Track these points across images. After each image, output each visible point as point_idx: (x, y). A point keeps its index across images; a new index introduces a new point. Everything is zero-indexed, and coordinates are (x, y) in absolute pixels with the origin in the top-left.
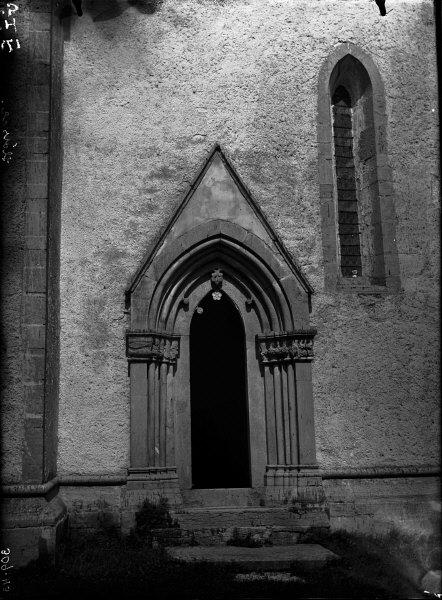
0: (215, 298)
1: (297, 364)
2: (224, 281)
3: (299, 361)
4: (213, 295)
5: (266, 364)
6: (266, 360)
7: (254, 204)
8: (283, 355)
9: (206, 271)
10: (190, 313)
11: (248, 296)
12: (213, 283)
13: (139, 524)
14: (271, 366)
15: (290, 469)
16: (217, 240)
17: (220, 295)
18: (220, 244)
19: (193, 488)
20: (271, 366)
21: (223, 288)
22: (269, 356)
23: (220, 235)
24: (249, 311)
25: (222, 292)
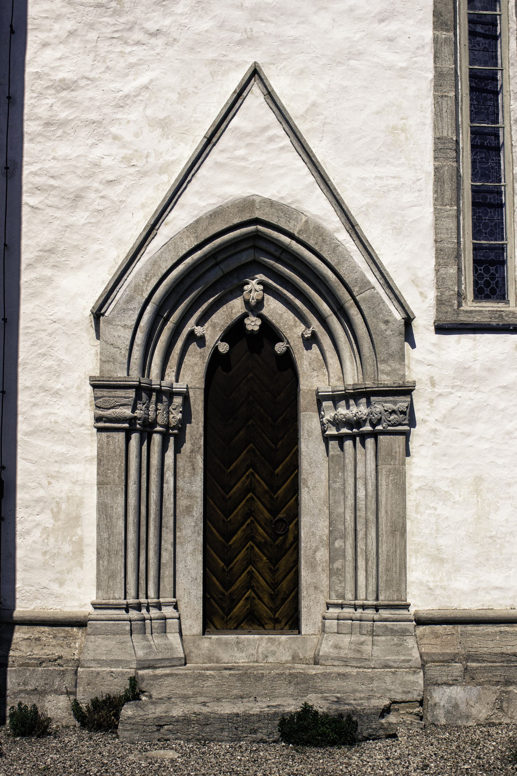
0: (249, 328)
1: (381, 438)
2: (266, 296)
3: (384, 433)
4: (247, 321)
5: (333, 437)
6: (332, 431)
7: (269, 93)
8: (359, 423)
9: (236, 282)
10: (208, 351)
11: (307, 325)
12: (247, 303)
13: (104, 702)
14: (341, 439)
15: (364, 607)
16: (251, 228)
17: (259, 322)
18: (257, 236)
19: (300, 633)
20: (341, 439)
21: (264, 311)
22: (337, 423)
23: (256, 221)
24: (308, 347)
25: (261, 317)
